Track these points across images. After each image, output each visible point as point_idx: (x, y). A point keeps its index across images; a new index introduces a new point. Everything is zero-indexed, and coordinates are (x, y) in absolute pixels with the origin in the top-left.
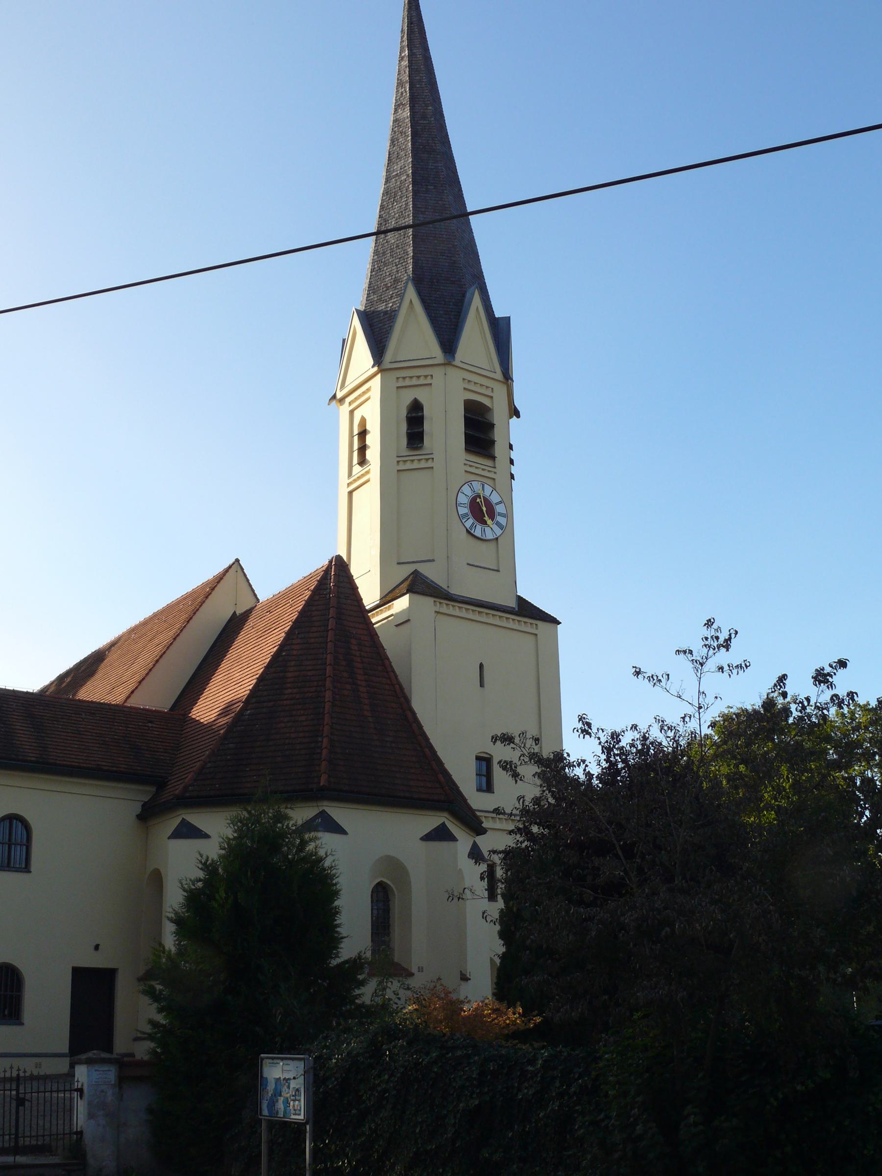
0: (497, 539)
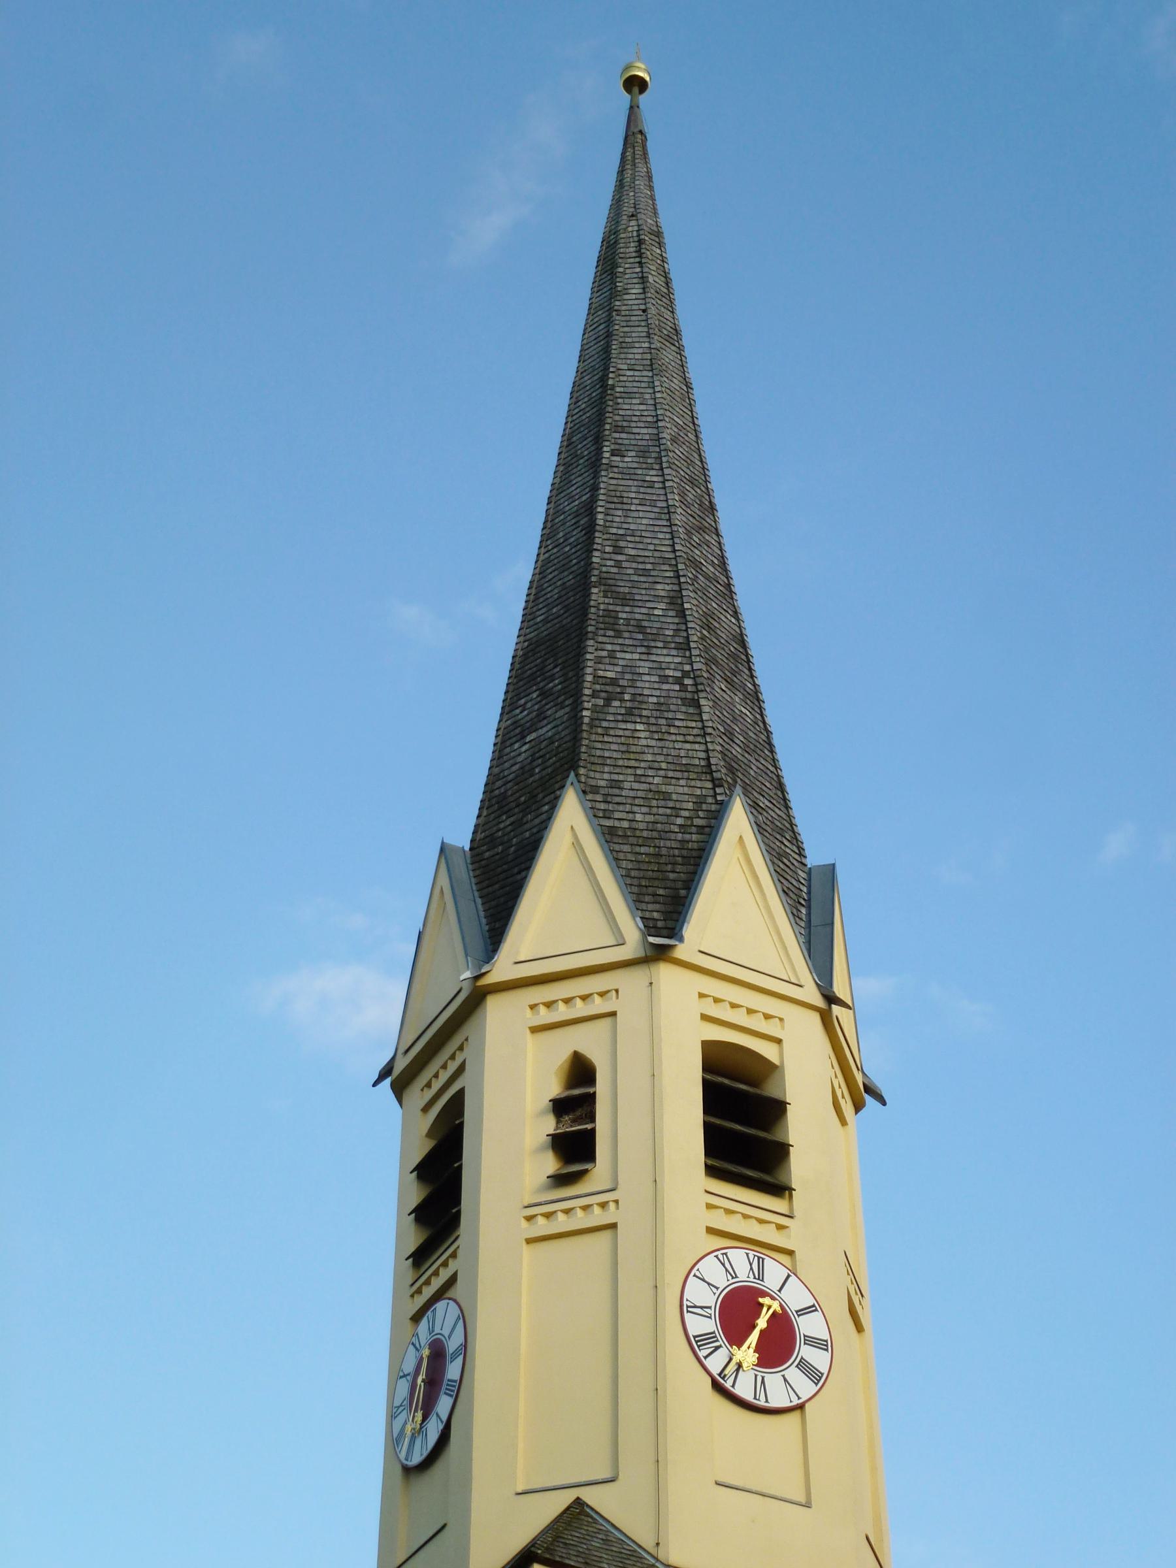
0: (801, 1407)
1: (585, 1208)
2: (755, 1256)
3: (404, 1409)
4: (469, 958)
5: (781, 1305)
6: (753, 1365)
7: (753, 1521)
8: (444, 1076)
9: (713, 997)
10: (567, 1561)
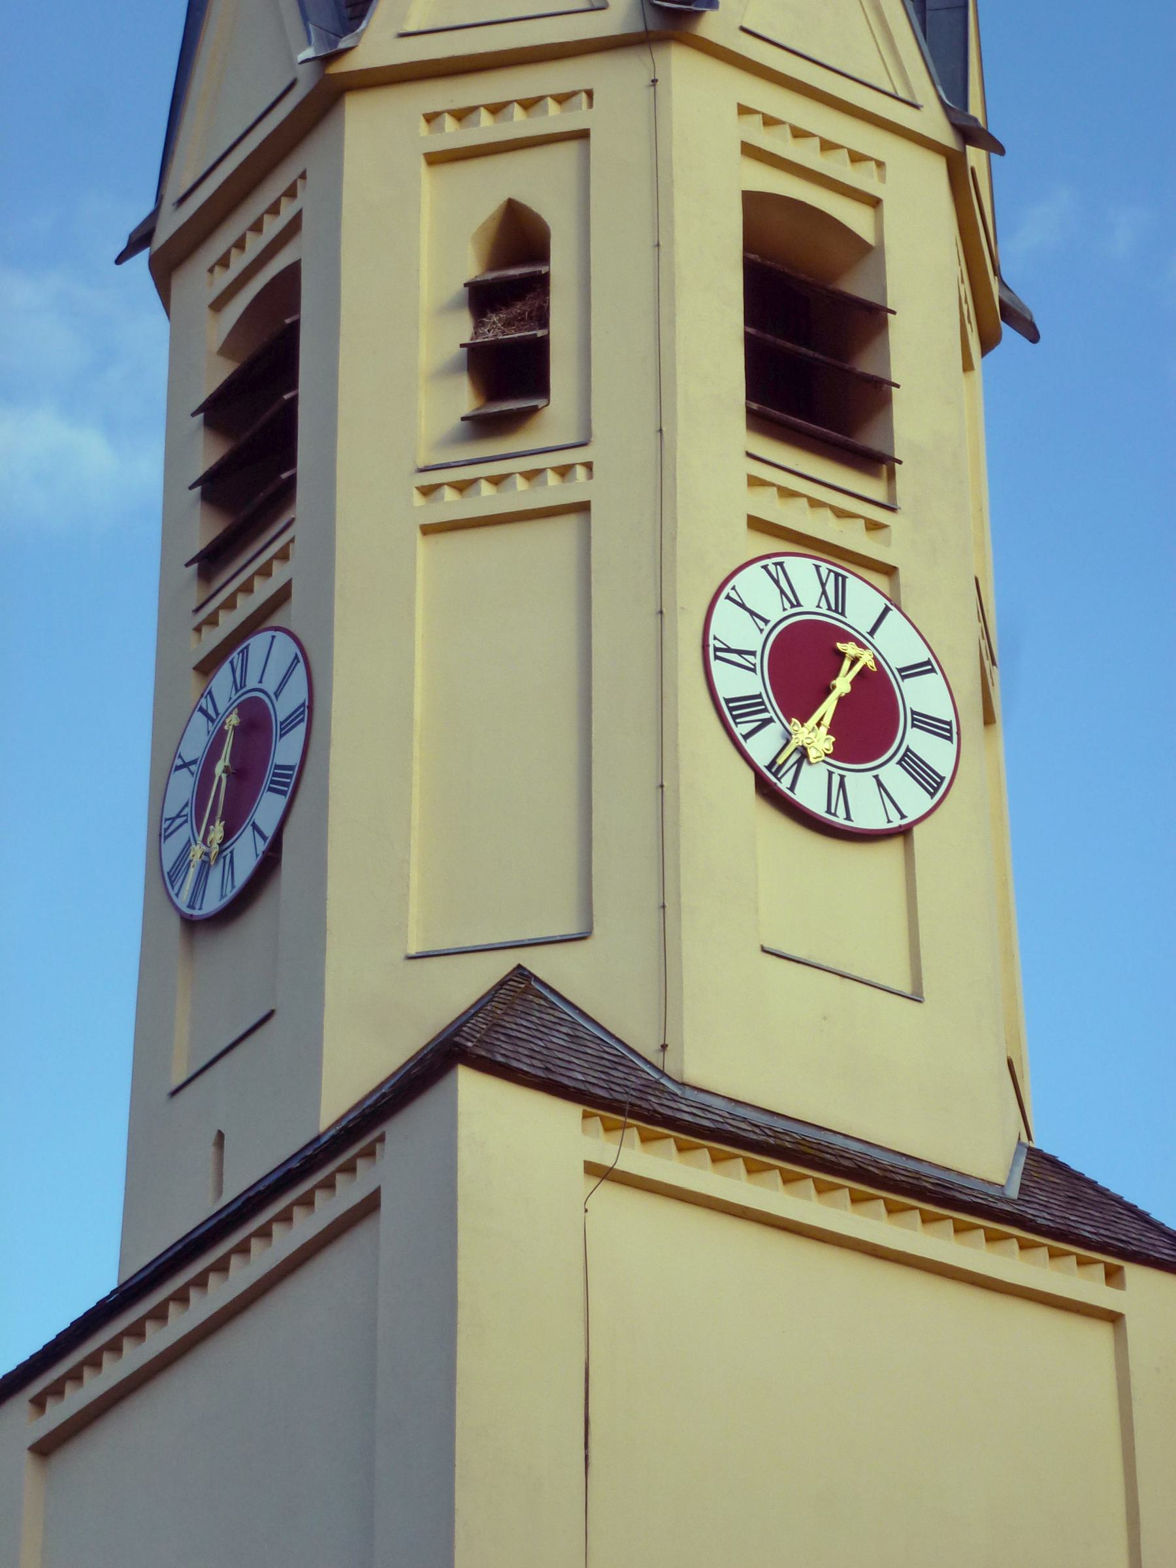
0: (904, 832)
1: (531, 475)
2: (830, 571)
3: (186, 821)
4: (311, 26)
5: (875, 658)
6: (826, 755)
7: (825, 1018)
8: (256, 245)
9: (763, 114)
10: (515, 1064)
